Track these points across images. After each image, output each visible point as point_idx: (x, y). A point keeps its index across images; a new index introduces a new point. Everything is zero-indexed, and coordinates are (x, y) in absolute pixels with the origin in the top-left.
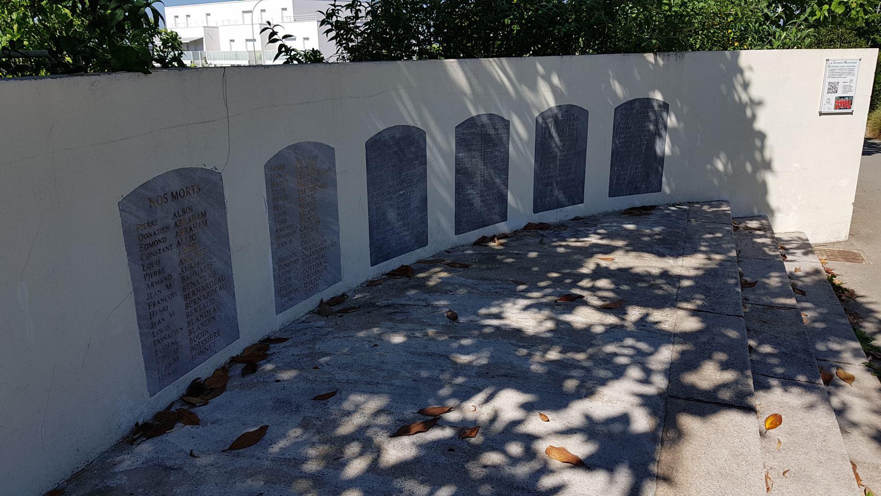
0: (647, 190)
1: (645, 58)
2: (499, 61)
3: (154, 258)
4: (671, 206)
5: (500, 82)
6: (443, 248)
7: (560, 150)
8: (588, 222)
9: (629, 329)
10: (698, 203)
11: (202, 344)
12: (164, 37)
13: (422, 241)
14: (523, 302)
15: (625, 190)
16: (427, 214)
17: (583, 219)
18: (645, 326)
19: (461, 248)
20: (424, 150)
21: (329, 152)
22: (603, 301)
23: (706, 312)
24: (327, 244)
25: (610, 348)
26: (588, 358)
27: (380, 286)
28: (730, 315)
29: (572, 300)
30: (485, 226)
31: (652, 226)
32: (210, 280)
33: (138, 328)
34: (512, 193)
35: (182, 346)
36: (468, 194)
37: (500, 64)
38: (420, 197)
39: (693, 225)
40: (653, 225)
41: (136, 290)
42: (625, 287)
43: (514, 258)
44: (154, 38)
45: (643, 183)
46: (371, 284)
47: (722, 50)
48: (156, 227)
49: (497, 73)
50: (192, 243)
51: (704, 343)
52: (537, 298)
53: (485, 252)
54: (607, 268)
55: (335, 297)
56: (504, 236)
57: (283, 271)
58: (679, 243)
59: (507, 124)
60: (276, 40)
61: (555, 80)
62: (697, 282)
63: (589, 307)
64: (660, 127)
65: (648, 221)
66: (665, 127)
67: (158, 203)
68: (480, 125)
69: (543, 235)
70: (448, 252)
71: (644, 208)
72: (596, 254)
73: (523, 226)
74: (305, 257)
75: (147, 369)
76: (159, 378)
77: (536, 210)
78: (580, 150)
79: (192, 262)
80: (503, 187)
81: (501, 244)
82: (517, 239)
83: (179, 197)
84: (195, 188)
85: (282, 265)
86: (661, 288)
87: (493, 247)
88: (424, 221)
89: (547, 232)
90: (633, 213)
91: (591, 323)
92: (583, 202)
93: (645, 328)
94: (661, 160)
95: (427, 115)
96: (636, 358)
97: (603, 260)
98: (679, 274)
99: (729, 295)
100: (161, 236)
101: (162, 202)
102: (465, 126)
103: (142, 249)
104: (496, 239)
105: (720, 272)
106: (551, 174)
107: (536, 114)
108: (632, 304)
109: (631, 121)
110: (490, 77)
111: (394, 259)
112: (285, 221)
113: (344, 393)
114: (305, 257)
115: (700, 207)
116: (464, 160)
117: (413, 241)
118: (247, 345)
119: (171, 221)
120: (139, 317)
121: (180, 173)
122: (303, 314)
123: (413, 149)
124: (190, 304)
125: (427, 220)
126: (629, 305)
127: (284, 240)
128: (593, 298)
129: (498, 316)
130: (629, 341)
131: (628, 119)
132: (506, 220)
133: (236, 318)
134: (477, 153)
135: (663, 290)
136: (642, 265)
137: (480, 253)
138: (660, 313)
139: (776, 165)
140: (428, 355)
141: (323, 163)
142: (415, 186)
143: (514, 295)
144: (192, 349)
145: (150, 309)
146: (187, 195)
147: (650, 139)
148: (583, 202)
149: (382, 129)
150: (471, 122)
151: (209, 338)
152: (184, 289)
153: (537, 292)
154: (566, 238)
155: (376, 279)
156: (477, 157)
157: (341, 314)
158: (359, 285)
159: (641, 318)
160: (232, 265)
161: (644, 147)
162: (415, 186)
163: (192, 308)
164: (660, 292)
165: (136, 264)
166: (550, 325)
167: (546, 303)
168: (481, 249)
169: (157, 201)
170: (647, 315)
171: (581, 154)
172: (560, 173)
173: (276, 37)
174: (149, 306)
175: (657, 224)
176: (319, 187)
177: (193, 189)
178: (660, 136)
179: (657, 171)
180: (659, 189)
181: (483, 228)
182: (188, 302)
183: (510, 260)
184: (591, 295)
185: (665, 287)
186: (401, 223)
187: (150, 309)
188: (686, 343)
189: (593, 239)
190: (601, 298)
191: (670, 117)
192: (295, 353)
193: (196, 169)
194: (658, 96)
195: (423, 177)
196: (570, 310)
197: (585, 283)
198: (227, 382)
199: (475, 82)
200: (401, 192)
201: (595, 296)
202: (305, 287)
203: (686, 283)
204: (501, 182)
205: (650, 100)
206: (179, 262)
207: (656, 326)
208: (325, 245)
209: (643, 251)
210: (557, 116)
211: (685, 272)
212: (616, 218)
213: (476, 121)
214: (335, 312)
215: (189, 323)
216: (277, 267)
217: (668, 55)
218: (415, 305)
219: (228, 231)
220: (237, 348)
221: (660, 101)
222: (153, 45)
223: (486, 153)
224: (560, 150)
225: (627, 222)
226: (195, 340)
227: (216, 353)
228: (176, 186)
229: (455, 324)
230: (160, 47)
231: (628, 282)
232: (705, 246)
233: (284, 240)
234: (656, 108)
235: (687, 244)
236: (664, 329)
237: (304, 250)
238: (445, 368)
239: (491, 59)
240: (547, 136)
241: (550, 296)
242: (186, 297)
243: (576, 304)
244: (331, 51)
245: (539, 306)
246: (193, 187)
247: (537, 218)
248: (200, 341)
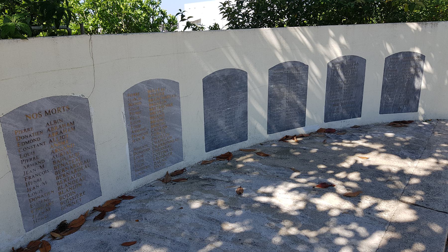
0: (407, 110)
1: (407, 26)
2: (302, 29)
3: (30, 151)
4: (424, 122)
5: (302, 42)
6: (258, 142)
7: (345, 84)
8: (362, 130)
9: (357, 215)
10: (444, 120)
11: (70, 200)
12: (169, 18)
13: (243, 137)
14: (292, 185)
15: (391, 109)
16: (247, 122)
17: (360, 127)
18: (370, 214)
19: (271, 142)
20: (246, 83)
21: (175, 85)
22: (348, 190)
23: (421, 206)
24: (172, 139)
25: (338, 230)
26: (316, 236)
27: (209, 165)
28: (439, 211)
29: (325, 187)
30: (289, 129)
31: (406, 135)
32: (77, 162)
33: (15, 192)
34: (308, 109)
35: (53, 202)
36: (277, 110)
37: (302, 31)
38: (243, 111)
39: (436, 136)
40: (407, 134)
41: (13, 170)
42: (368, 180)
43: (300, 152)
44: (164, 19)
45: (405, 106)
46: (204, 163)
47: (384, 23)
48: (32, 132)
49: (301, 38)
50: (62, 141)
51: (410, 233)
52: (303, 183)
53: (284, 146)
54: (361, 164)
55: (178, 170)
56: (302, 136)
57: (137, 155)
58: (420, 149)
59: (306, 68)
60: (185, 20)
61: (343, 40)
62: (422, 181)
63: (335, 194)
64: (419, 70)
65: (404, 131)
66: (422, 71)
67: (33, 117)
68: (286, 68)
69: (328, 137)
70: (262, 145)
71: (404, 122)
72: (358, 153)
73: (316, 130)
74: (154, 147)
75: (23, 216)
76: (34, 221)
77: (326, 120)
78: (359, 84)
79: (61, 152)
80: (302, 106)
81: (298, 142)
82: (310, 138)
83: (51, 114)
84: (65, 108)
86: (394, 183)
87: (291, 143)
88: (245, 125)
89: (332, 134)
90: (395, 125)
91: (331, 207)
92: (360, 117)
93: (369, 215)
94: (418, 92)
95: (248, 62)
96: (353, 241)
97: (361, 159)
98: (411, 173)
99: (444, 194)
100: (35, 137)
101: (37, 117)
102: (276, 69)
103: (20, 145)
104: (295, 138)
105: (443, 174)
106: (337, 99)
107: (328, 61)
108: (367, 195)
109: (397, 66)
110: (295, 39)
111: (222, 148)
112: (139, 126)
113: (142, 242)
114: (154, 147)
115: (445, 123)
116: (275, 89)
117: (237, 138)
118: (108, 199)
119: (44, 128)
120: (17, 186)
121: (52, 99)
122: (153, 181)
123: (238, 83)
124: (60, 177)
125: (247, 125)
126: (365, 195)
127: (138, 137)
128: (341, 187)
129: (270, 195)
130: (354, 226)
131: (395, 65)
132: (304, 126)
133: (99, 184)
134: (284, 85)
135: (395, 185)
136: (387, 164)
137: (281, 147)
138: (385, 204)
140: (209, 220)
141: (170, 91)
142: (238, 105)
143: (288, 179)
144: (61, 203)
145: (26, 180)
146: (58, 112)
147: (410, 78)
148: (360, 117)
149: (215, 71)
150: (280, 66)
151: (76, 196)
152: (55, 168)
153: (304, 178)
154: (343, 140)
155: (209, 160)
156: (284, 88)
157: (175, 182)
158: (197, 163)
159: (369, 207)
160: (96, 153)
161: (406, 83)
162: (238, 105)
163: (62, 179)
164: (391, 186)
165: (14, 154)
166: (301, 205)
167: (307, 187)
168: (283, 144)
169: (33, 116)
170: (376, 204)
171: (361, 86)
172: (344, 98)
173: (184, 18)
174: (25, 179)
175: (409, 134)
176: (166, 106)
177: (64, 109)
178: (418, 76)
179: (415, 98)
180: (416, 110)
181: (287, 131)
182: (59, 176)
183: (297, 153)
184: (341, 185)
185: (398, 183)
186: (228, 127)
187: (26, 180)
188: (396, 232)
189: (360, 143)
190: (347, 188)
191: (425, 64)
192: (132, 208)
193: (67, 96)
194: (417, 51)
195: (245, 99)
196: (319, 195)
197: (341, 175)
198: (83, 224)
199: (283, 41)
200: (228, 109)
201: (343, 185)
202: (155, 165)
203: (414, 181)
204: (301, 103)
205: (411, 53)
206: (51, 152)
207: (379, 215)
208: (171, 140)
209: (392, 154)
210: (343, 63)
211: (416, 172)
212: (383, 127)
213: (283, 66)
214: (172, 181)
215: (59, 188)
216: (132, 153)
217: (426, 24)
218: (221, 181)
219: (93, 133)
220: (99, 202)
221: (419, 53)
222: (163, 22)
223: (290, 85)
224: (345, 84)
225: (389, 131)
226: (64, 197)
227: (81, 205)
228: (49, 107)
229: (239, 197)
230: (167, 23)
231: (372, 177)
232: (439, 153)
233: (138, 137)
234: (416, 58)
235: (426, 150)
236: (383, 218)
237: (153, 143)
238: (214, 232)
239: (296, 28)
240: (335, 75)
241: (312, 182)
242: (56, 173)
243: (328, 190)
244: (223, 23)
245: (300, 190)
246: (63, 107)
247: (327, 125)
248: (68, 198)
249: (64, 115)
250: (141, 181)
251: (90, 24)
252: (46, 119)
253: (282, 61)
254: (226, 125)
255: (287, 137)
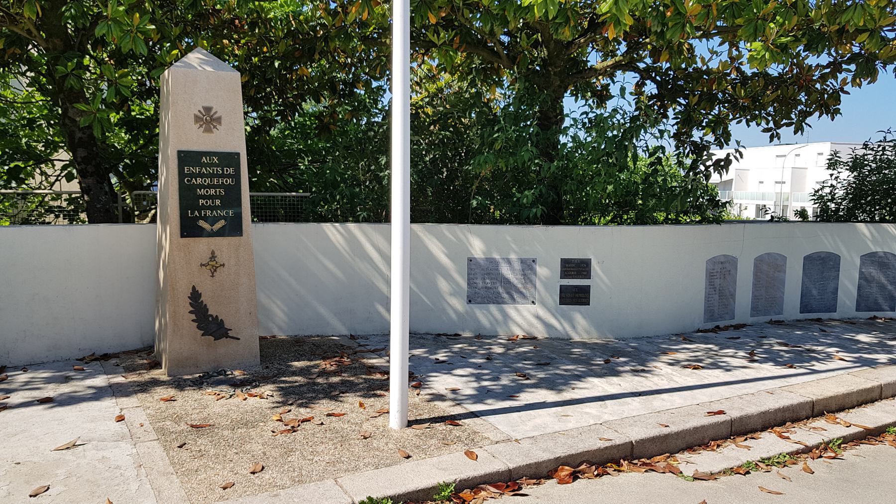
41: (706, 288)
85: (755, 298)
88: (835, 299)
100: (715, 274)
112: (759, 281)
120: (705, 297)
139: (206, 134)
215: (719, 305)
228: (722, 260)
242: (719, 296)
249: (727, 265)
250: (755, 319)
251: (589, 117)
252: (720, 266)
253: (874, 249)
254: (818, 296)
255: (875, 318)
